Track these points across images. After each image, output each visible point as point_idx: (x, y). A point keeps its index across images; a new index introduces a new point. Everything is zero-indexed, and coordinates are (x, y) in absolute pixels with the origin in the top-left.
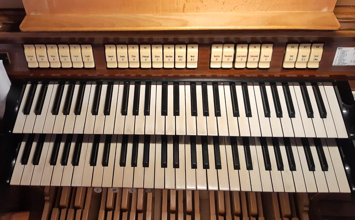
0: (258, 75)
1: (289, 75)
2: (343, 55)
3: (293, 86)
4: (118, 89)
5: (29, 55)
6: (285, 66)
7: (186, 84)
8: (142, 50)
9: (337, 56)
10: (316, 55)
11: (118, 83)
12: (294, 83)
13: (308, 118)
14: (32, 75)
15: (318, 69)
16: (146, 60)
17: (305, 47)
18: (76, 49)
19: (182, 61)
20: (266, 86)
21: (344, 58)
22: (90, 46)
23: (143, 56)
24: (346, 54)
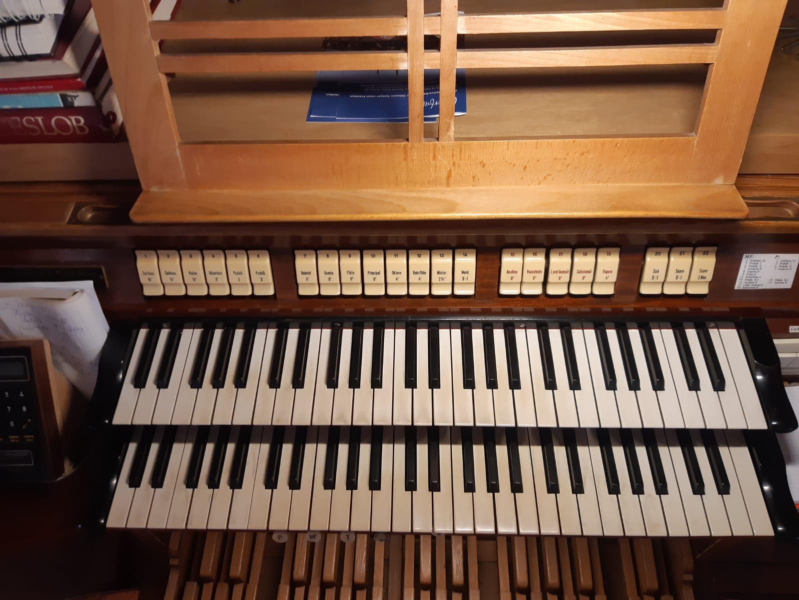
2: (755, 268)
4: (320, 338)
5: (145, 272)
6: (645, 290)
7: (323, 326)
8: (368, 261)
9: (744, 271)
11: (320, 326)
12: (661, 324)
14: (150, 310)
21: (756, 276)
22: (266, 252)
23: (368, 272)
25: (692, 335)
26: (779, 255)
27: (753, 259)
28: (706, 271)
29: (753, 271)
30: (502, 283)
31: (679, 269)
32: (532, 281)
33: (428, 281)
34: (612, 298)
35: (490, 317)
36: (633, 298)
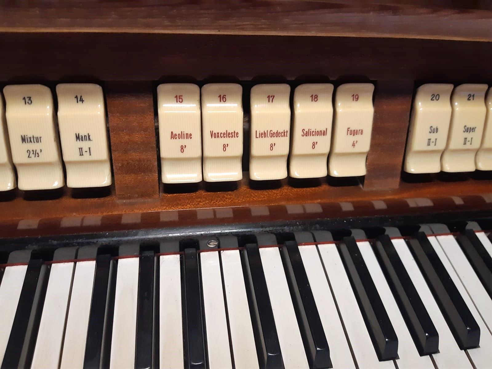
0: (385, 201)
1: (420, 200)
3: (315, 246)
6: (414, 167)
7: (78, 258)
12: (317, 234)
15: (117, 191)
16: (182, 148)
17: (471, 98)
18: (26, 105)
19: (95, 156)
20: (300, 248)
22: (97, 89)
30: (207, 158)
31: (469, 126)
32: (222, 154)
34: (361, 186)
35: (197, 230)
36: (395, 182)
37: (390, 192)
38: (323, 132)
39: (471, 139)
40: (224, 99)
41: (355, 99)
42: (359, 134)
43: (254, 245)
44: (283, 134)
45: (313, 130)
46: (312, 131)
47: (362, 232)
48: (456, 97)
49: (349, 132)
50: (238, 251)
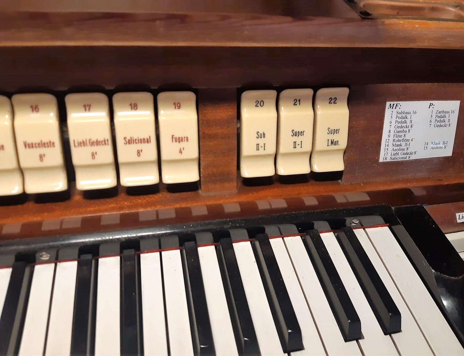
2: (403, 125)
6: (248, 171)
7: (59, 259)
8: (122, 115)
9: (390, 131)
10: (332, 128)
12: (283, 227)
13: (346, 341)
16: (139, 153)
17: (298, 103)
21: (406, 138)
22: (191, 96)
24: (449, 120)
25: (329, 239)
26: (433, 102)
27: (400, 111)
28: (336, 131)
29: (402, 129)
31: (296, 130)
33: (154, 157)
36: (233, 186)
37: (227, 196)
38: (146, 140)
39: (301, 142)
40: (37, 110)
41: (177, 107)
42: (185, 141)
43: (192, 243)
44: (105, 142)
45: (135, 137)
46: (134, 139)
47: (326, 224)
48: (317, 102)
49: (174, 139)
50: (249, 242)
